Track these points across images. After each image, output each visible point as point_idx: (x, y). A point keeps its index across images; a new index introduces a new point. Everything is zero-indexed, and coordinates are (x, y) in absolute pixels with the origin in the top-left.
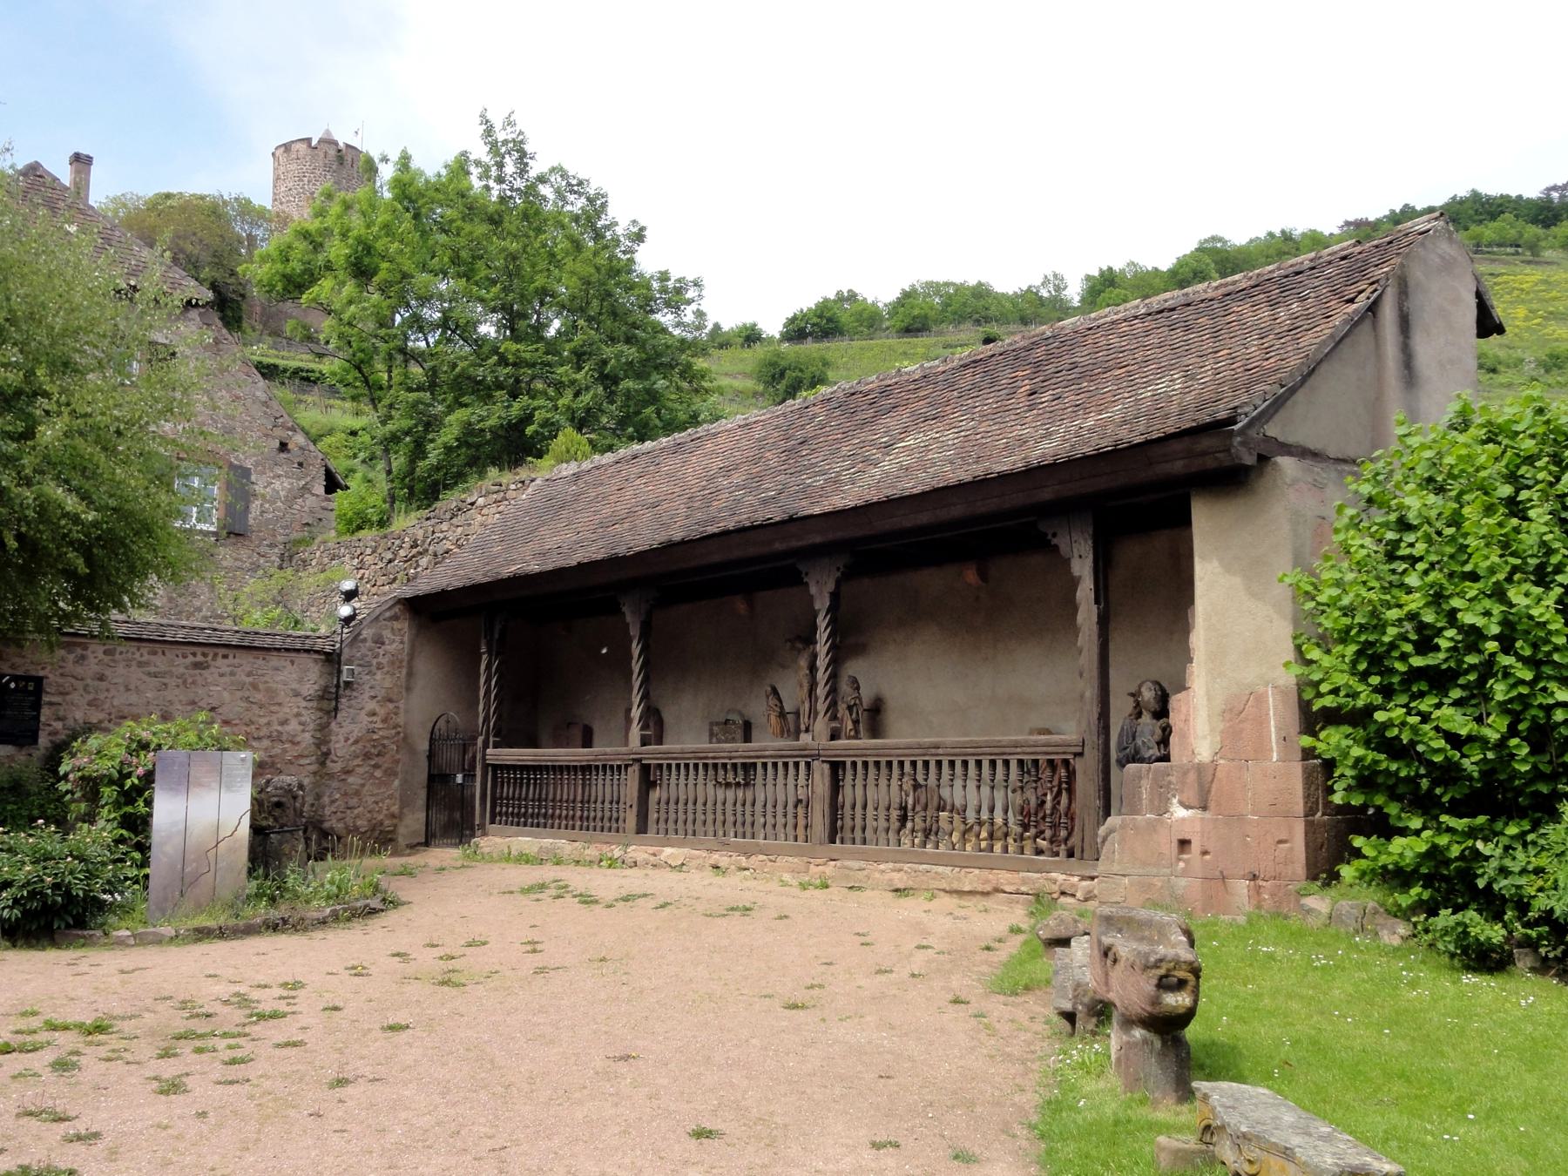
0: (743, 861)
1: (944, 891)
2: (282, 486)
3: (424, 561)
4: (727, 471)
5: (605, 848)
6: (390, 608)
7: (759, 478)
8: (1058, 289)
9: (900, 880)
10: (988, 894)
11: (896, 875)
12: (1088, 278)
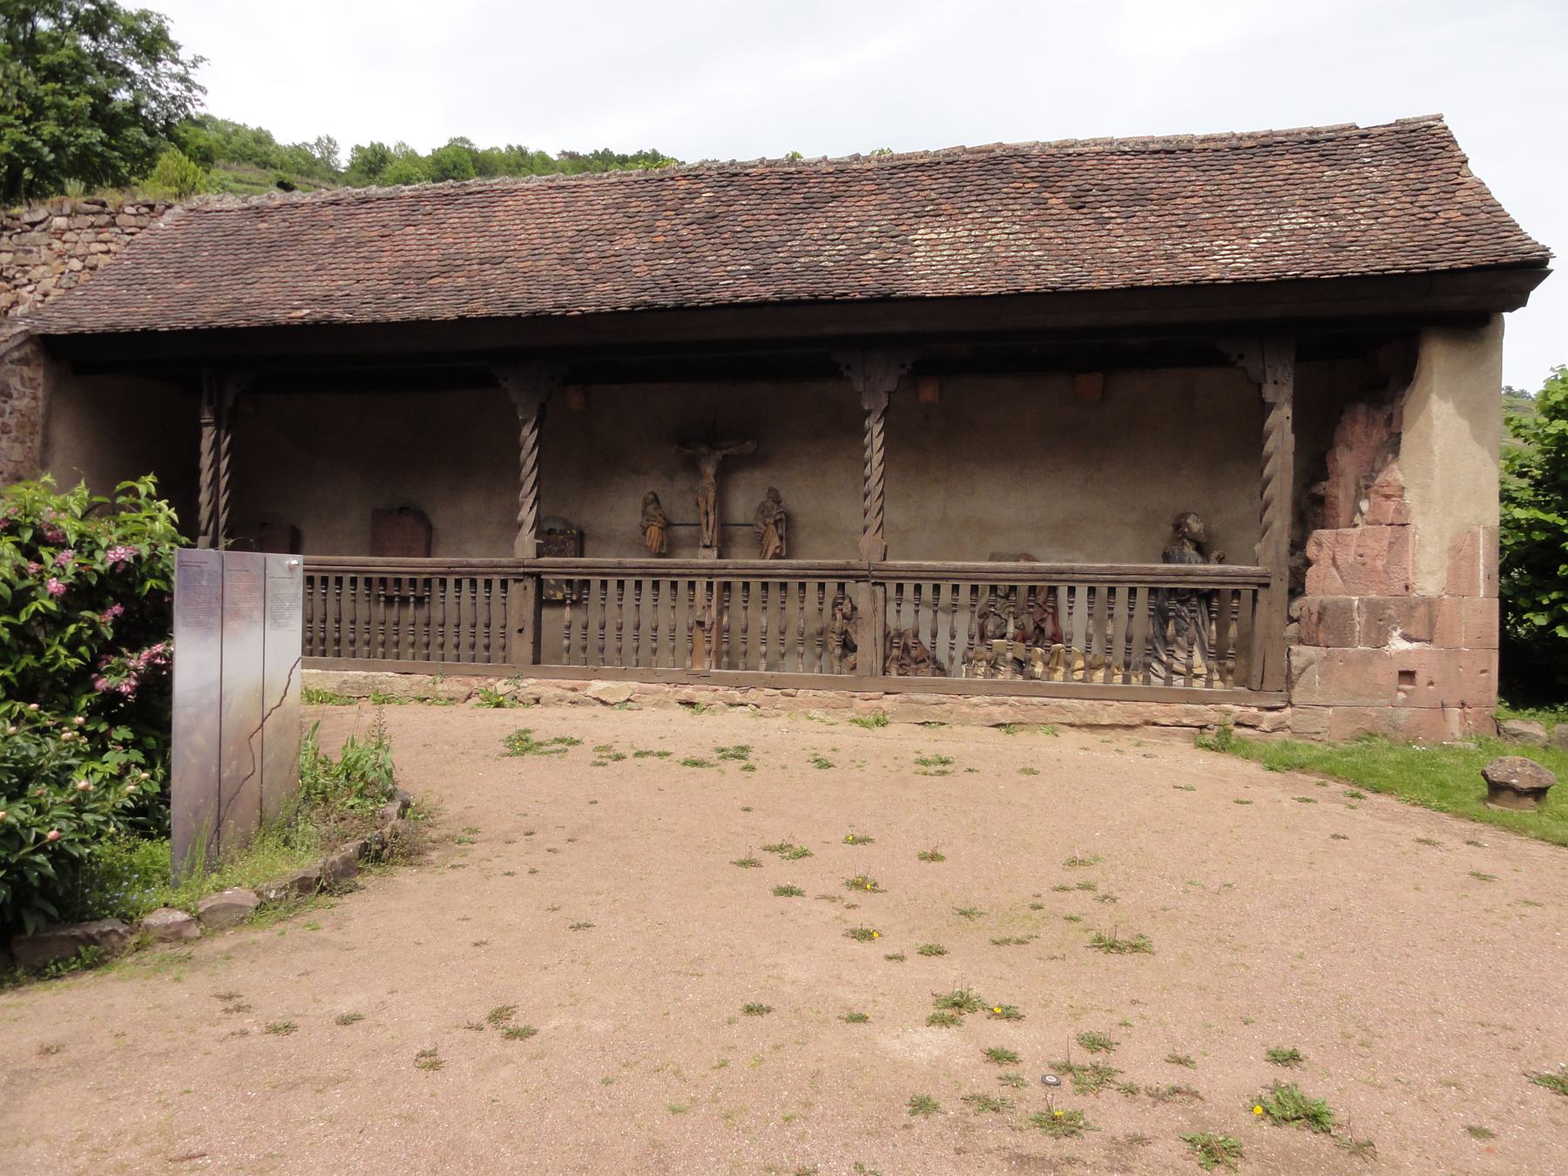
0: (737, 696)
1: (1071, 725)
5: (474, 682)
6: (18, 348)
8: (332, 152)
9: (1004, 714)
10: (1147, 723)
11: (995, 709)
12: (358, 149)
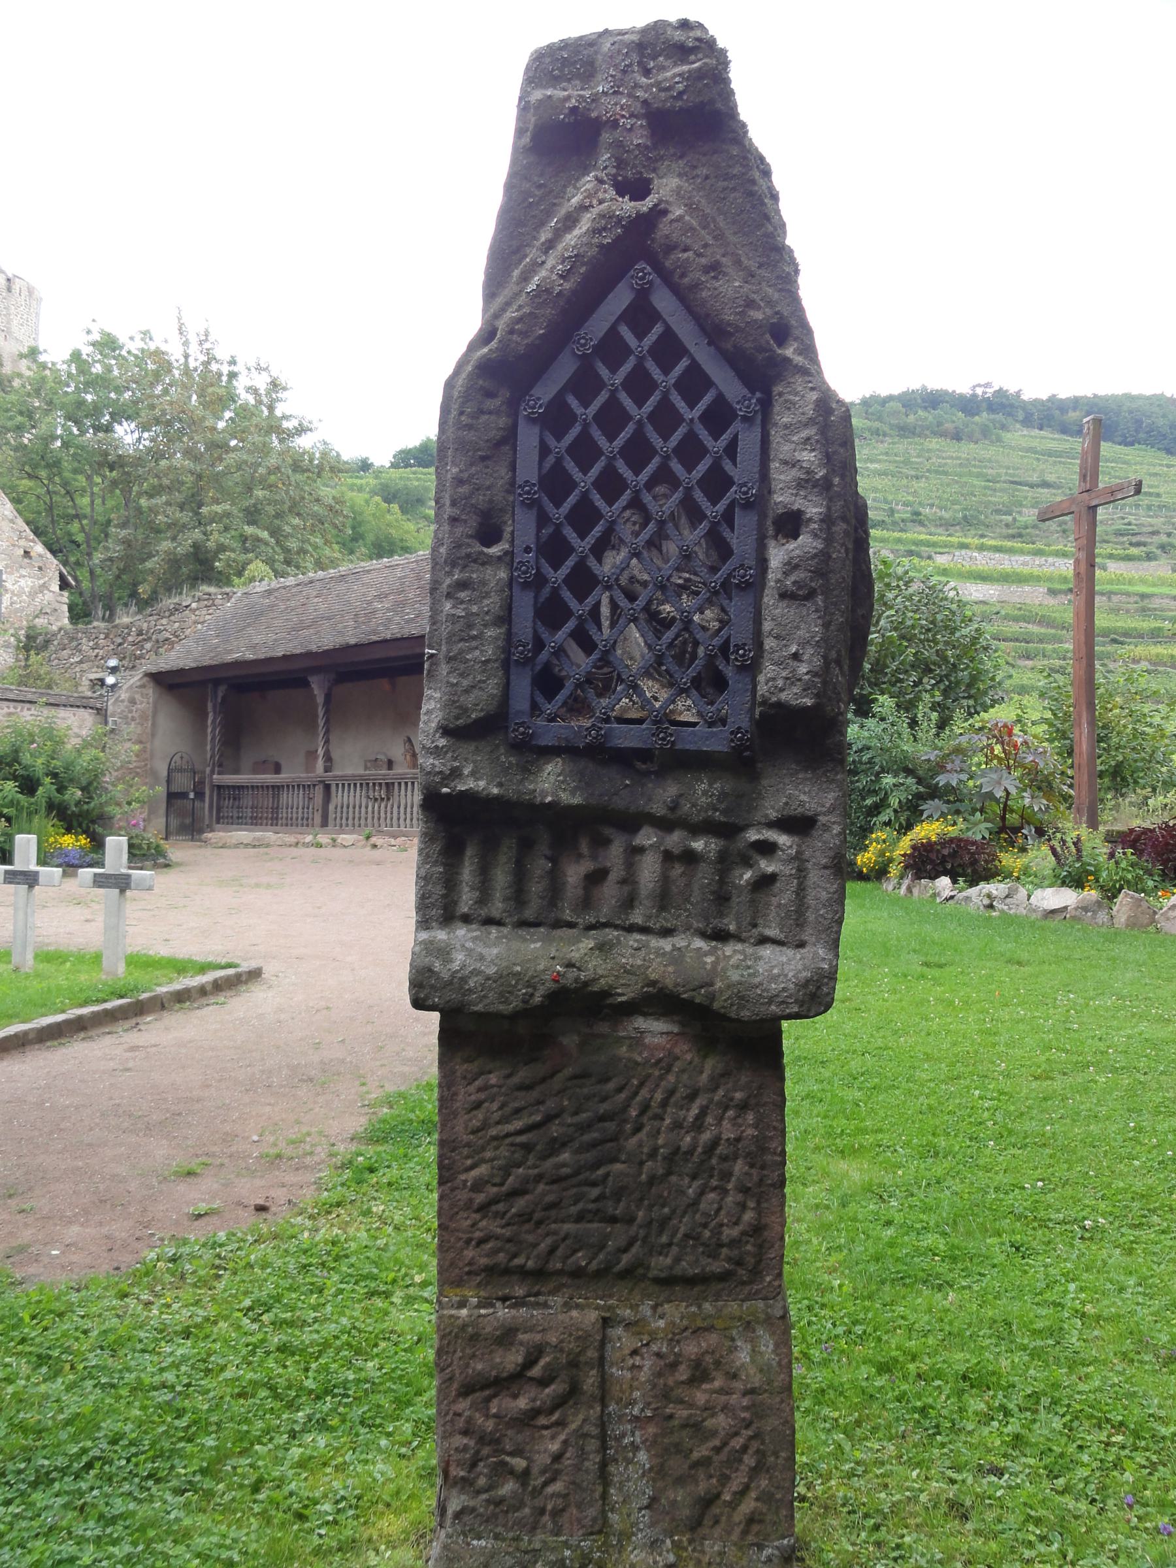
0: (393, 841)
2: (27, 583)
3: (148, 646)
4: (380, 597)
7: (403, 603)
